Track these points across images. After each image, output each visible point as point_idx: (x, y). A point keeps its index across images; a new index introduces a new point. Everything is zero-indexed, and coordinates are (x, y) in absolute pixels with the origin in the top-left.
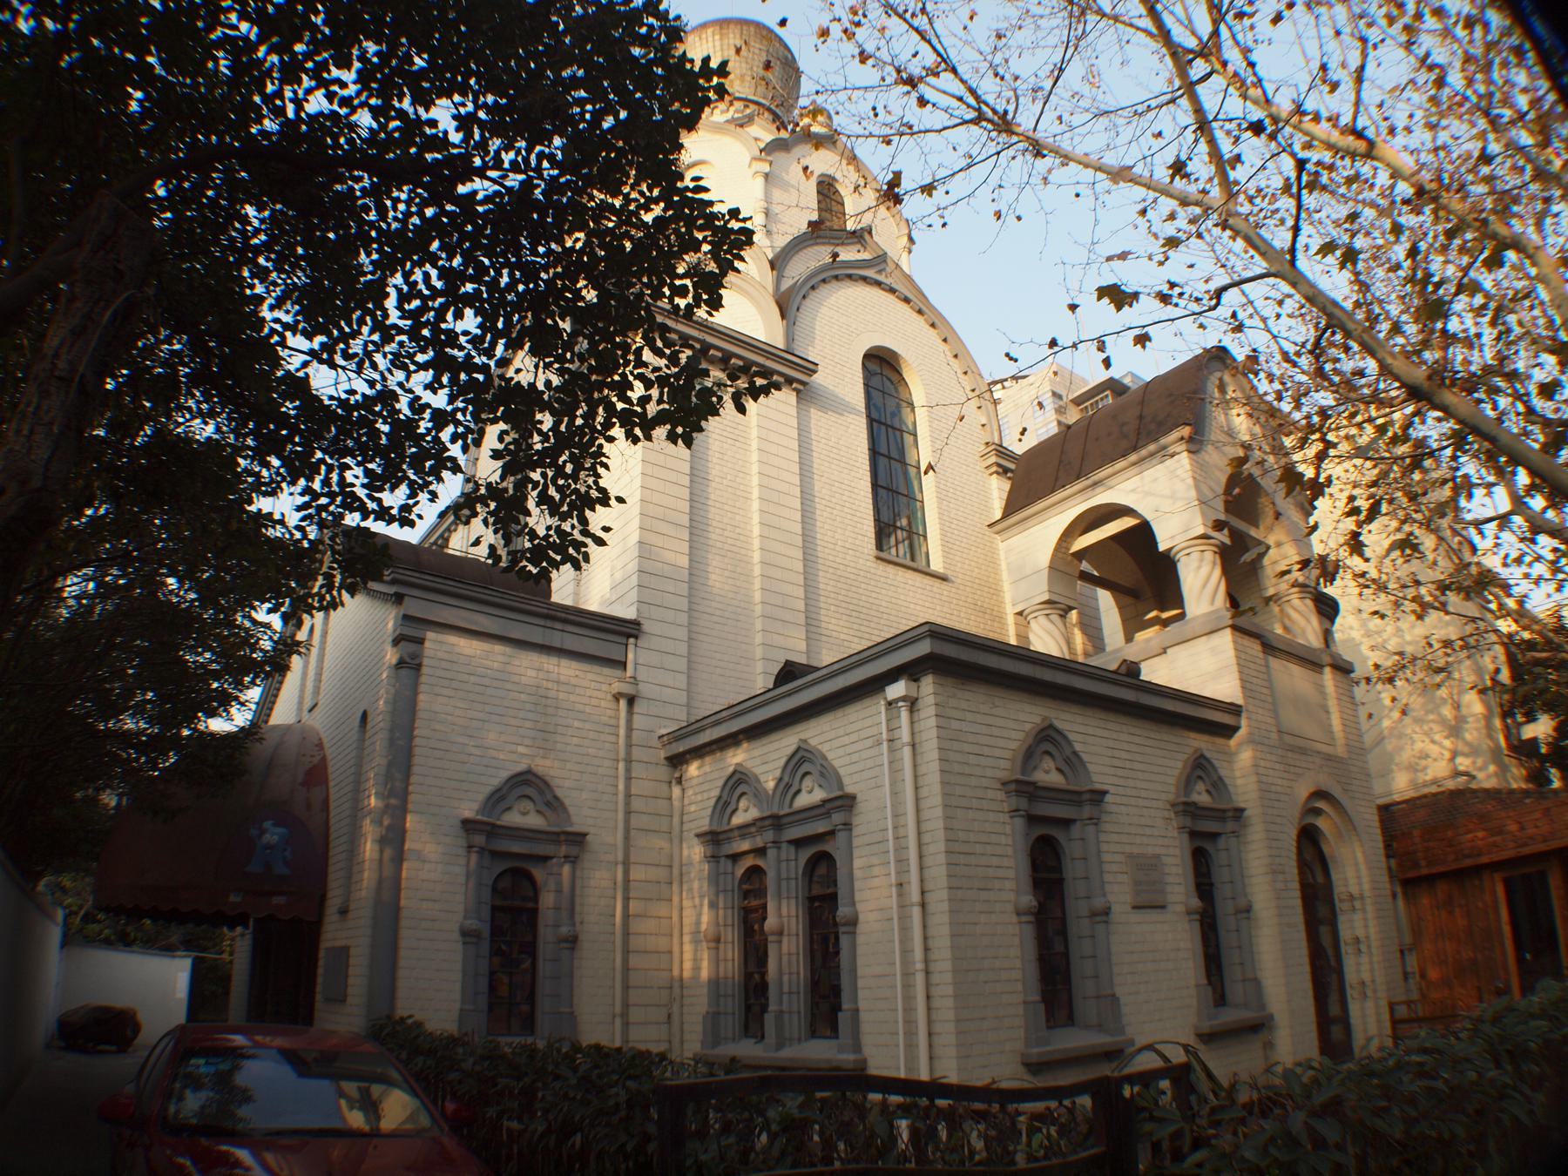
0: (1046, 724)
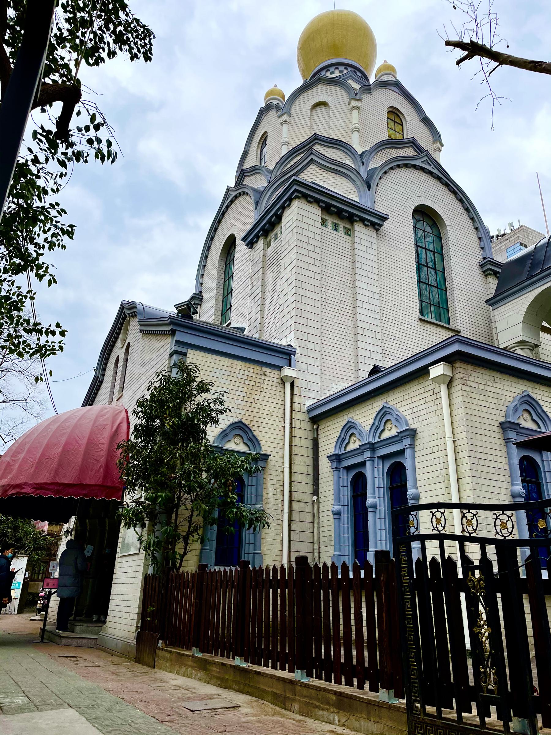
0: (525, 394)
